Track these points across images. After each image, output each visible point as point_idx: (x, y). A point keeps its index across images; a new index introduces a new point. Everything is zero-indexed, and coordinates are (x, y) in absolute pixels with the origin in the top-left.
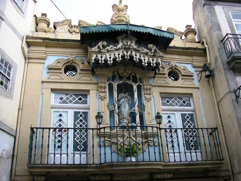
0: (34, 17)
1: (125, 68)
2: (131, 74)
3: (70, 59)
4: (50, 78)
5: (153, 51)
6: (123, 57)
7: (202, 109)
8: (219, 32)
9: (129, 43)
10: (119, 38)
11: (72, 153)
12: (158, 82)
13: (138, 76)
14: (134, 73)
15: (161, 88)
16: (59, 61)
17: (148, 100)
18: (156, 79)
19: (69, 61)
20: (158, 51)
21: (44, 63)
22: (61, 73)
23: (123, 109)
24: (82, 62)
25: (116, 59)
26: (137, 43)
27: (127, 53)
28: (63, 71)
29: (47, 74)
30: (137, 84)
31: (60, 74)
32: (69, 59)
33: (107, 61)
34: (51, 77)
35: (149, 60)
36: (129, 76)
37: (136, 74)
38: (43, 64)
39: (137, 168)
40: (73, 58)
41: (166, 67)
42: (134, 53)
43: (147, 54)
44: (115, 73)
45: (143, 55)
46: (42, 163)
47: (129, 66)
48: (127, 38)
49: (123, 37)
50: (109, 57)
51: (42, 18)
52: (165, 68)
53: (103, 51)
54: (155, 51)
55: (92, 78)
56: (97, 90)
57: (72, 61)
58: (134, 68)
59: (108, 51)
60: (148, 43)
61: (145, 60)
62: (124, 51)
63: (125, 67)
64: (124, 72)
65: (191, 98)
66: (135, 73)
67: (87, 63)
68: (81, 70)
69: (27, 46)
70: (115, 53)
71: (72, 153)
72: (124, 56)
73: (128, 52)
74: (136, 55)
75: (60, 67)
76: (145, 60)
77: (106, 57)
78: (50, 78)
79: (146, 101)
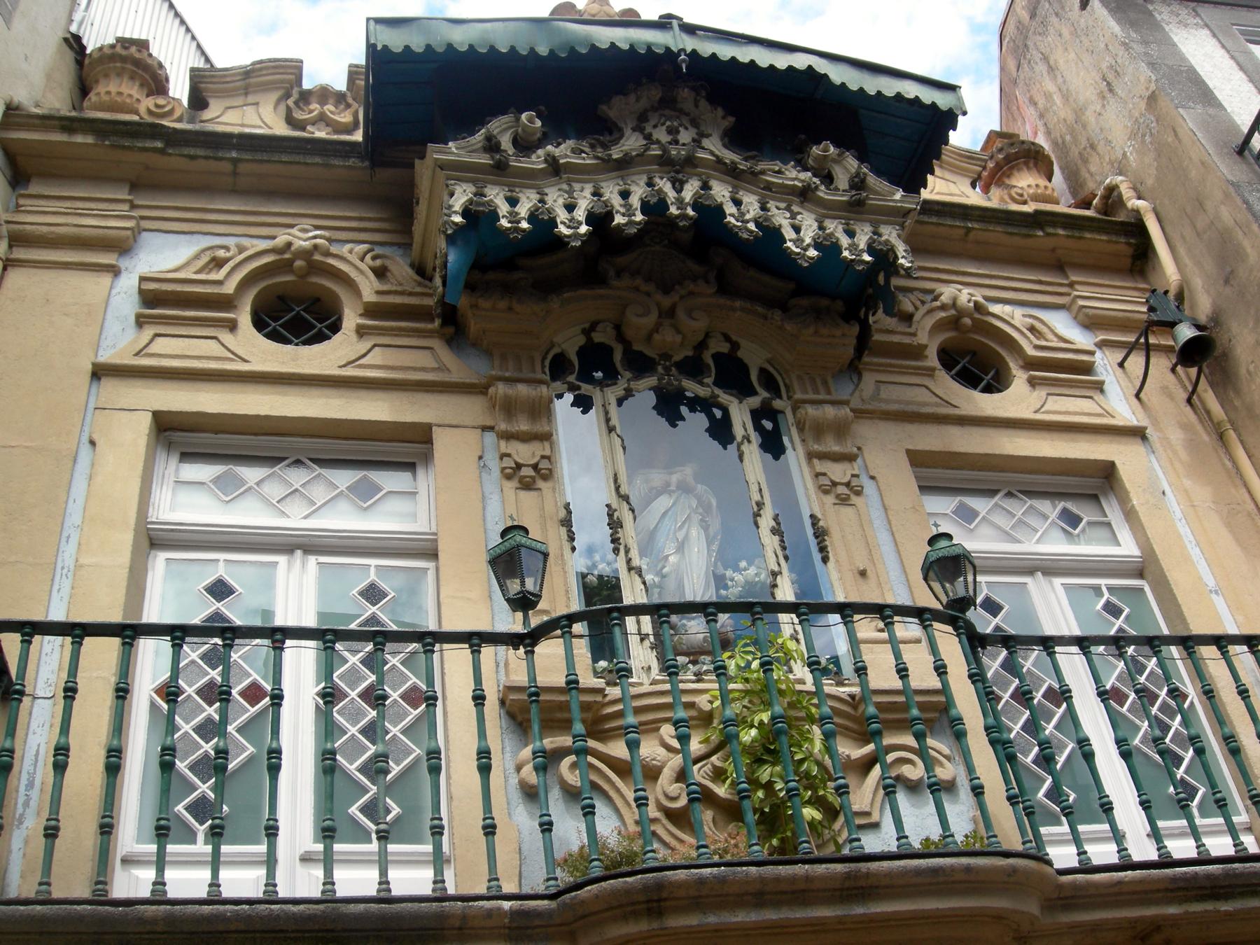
0: (71, 47)
1: (666, 302)
2: (702, 346)
4: (155, 348)
5: (842, 181)
6: (657, 208)
7: (1195, 553)
8: (1211, 111)
9: (685, 136)
10: (615, 109)
11: (306, 859)
12: (888, 392)
13: (754, 357)
14: (727, 338)
15: (912, 428)
16: (221, 253)
17: (841, 490)
18: (869, 380)
19: (287, 256)
20: (872, 180)
21: (115, 271)
22: (232, 326)
23: (672, 559)
24: (378, 262)
25: (609, 215)
26: (733, 139)
27: (678, 186)
28: (244, 318)
29: (131, 331)
30: (755, 402)
31: (226, 337)
33: (553, 223)
34: (161, 345)
35: (821, 228)
36: (690, 353)
37: (735, 346)
38: (111, 275)
39: (859, 910)
40: (318, 241)
41: (923, 310)
42: (721, 192)
43: (804, 195)
44: (598, 337)
45: (783, 205)
46: (57, 894)
47: (691, 294)
48: (667, 112)
49: (644, 103)
50: (561, 201)
51: (124, 53)
52: (917, 317)
53: (524, 163)
54: (858, 184)
55: (446, 355)
56: (485, 429)
57: (306, 254)
58: (722, 301)
59: (555, 169)
60: (803, 137)
61: (797, 229)
62: (657, 180)
63: (667, 290)
64: (657, 328)
65: (1106, 495)
66: (734, 338)
67: (410, 272)
68: (371, 311)
69: (8, 172)
70: (603, 184)
71: (306, 859)
72: (662, 204)
73: (682, 183)
74: (738, 203)
75: (230, 288)
76: (797, 229)
77: (542, 201)
78: (155, 348)
79: (830, 499)
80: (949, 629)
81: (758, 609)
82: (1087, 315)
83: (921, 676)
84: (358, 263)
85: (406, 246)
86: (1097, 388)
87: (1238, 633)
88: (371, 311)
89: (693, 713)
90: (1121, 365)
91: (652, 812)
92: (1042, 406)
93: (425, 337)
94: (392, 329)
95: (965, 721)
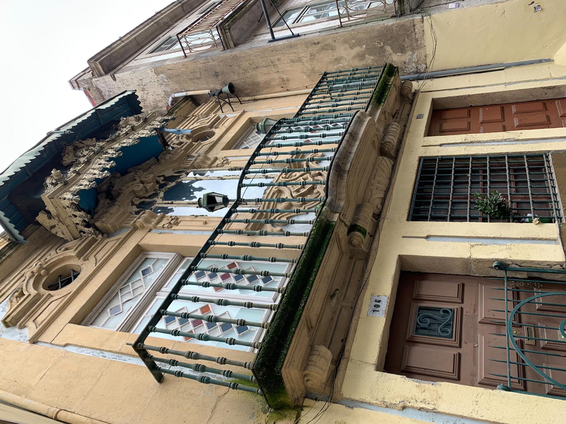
3: (35, 272)
32: (32, 272)
34: (40, 319)
37: (163, 176)
66: (161, 175)
68: (79, 255)
80: (219, 235)
81: (202, 254)
82: (204, 114)
83: (249, 216)
84: (58, 254)
85: (66, 241)
86: (50, 297)
87: (149, 335)
88: (79, 255)
89: (276, 195)
90: (223, 112)
91: (302, 209)
92: (96, 260)
93: (102, 243)
94: (92, 250)
95: (192, 351)
